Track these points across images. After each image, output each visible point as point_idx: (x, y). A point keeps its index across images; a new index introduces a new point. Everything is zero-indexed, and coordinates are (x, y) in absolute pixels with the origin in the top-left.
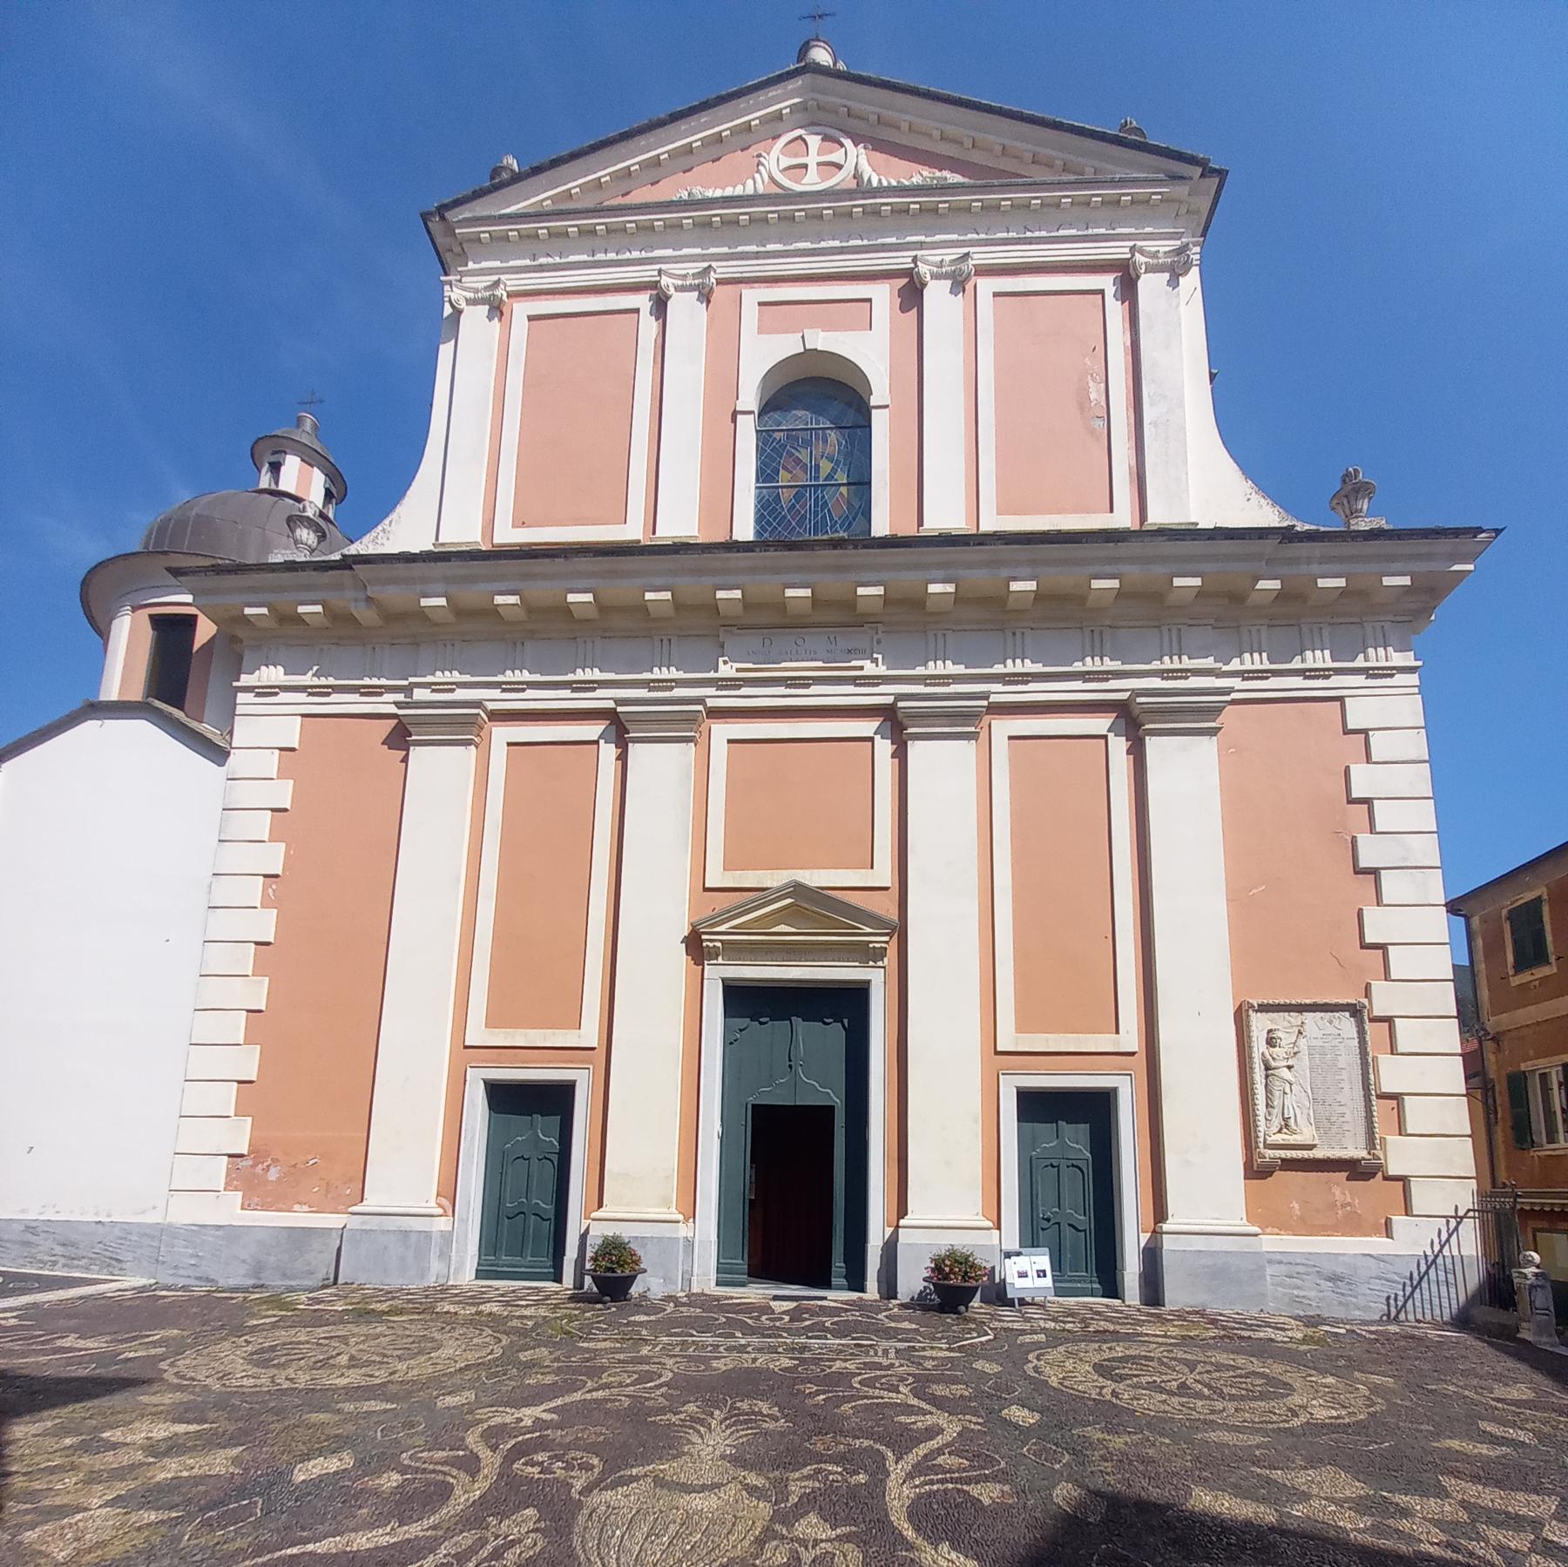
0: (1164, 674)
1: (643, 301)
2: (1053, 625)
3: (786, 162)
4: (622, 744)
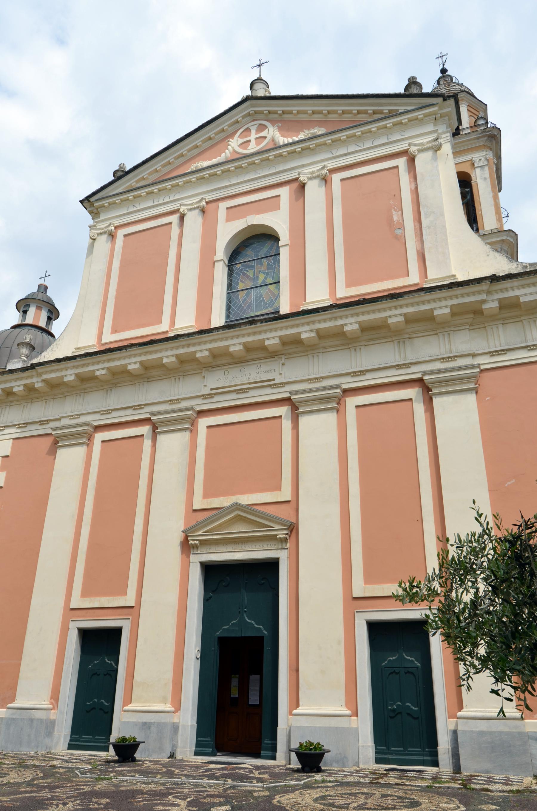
2: (376, 342)
3: (241, 141)
4: (429, 402)
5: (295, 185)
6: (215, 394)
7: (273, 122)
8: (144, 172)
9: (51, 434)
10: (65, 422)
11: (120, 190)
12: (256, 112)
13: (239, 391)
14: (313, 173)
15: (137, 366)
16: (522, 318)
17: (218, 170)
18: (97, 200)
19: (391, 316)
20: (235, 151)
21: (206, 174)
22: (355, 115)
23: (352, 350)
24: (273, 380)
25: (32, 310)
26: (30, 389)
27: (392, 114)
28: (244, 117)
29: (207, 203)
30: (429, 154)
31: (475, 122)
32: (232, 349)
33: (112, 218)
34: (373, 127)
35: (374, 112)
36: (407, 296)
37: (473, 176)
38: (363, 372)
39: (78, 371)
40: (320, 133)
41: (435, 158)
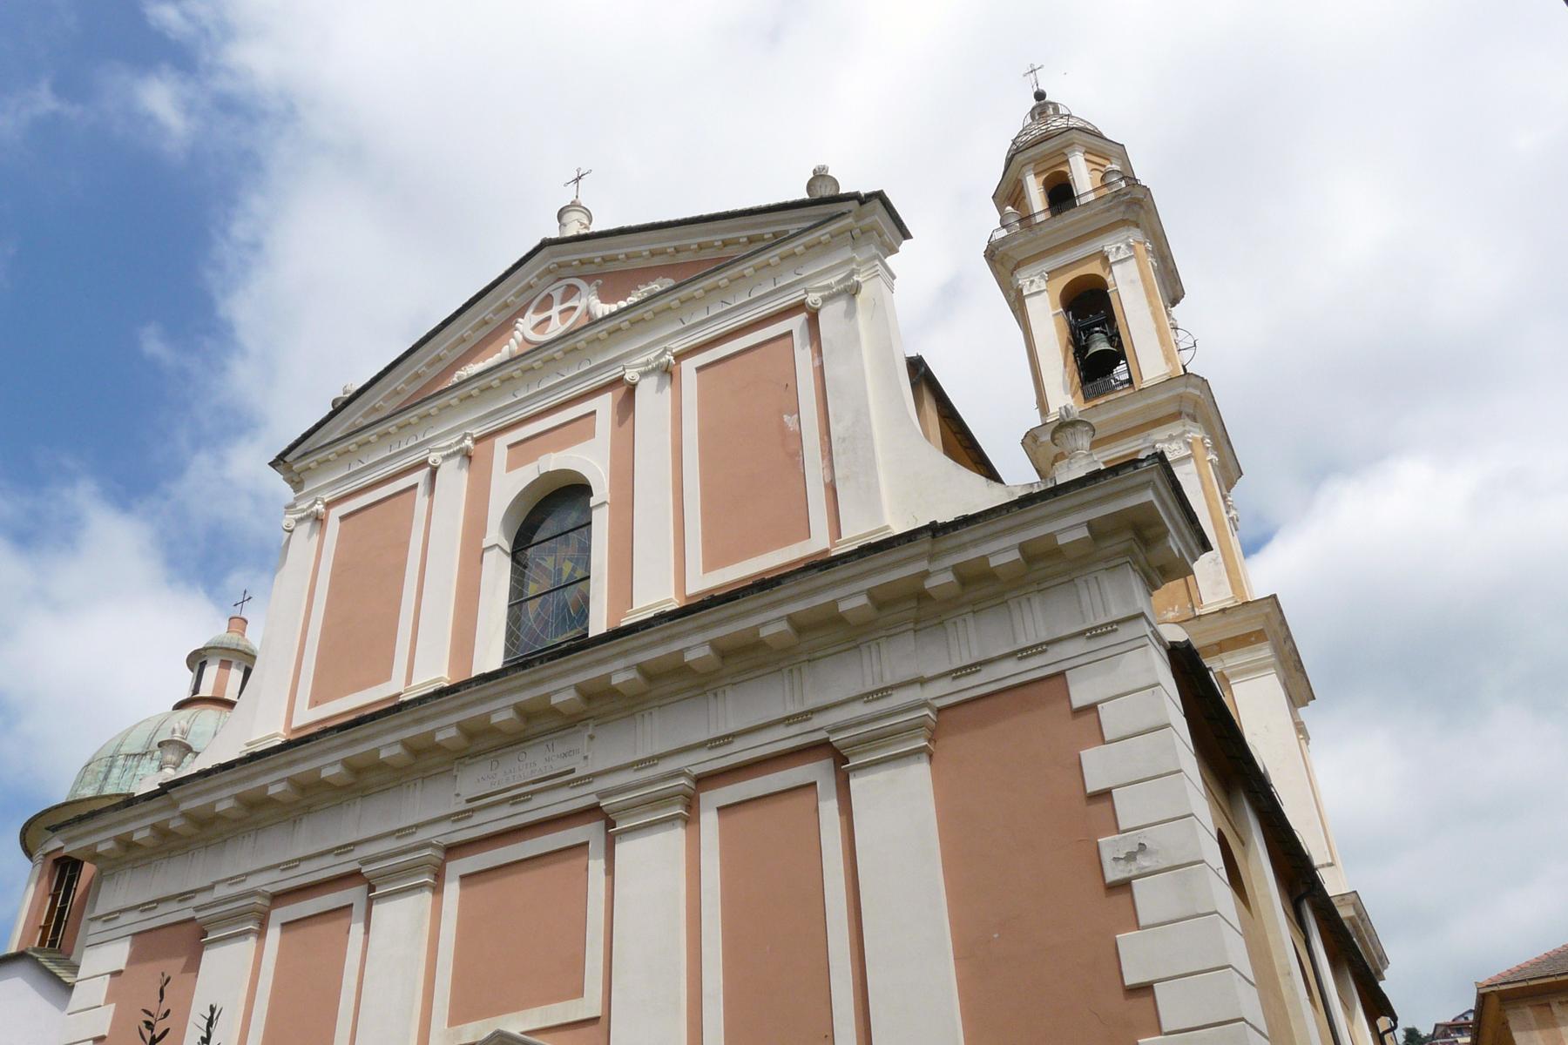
0: (232, 881)
1: (796, 323)
5: (621, 391)
6: (473, 810)
7: (589, 278)
8: (376, 398)
9: (192, 920)
10: (222, 892)
11: (337, 435)
12: (560, 266)
13: (515, 800)
14: (648, 363)
15: (453, 732)
16: (1074, 575)
17: (493, 380)
18: (305, 454)
19: (764, 624)
20: (526, 340)
21: (472, 389)
22: (695, 251)
23: (711, 697)
24: (573, 771)
25: (211, 671)
26: (162, 832)
27: (780, 239)
28: (539, 277)
29: (477, 441)
30: (840, 305)
31: (1102, 179)
32: (495, 719)
33: (323, 488)
34: (747, 268)
35: (751, 240)
36: (787, 583)
37: (1109, 280)
38: (883, 692)
39: (239, 790)
40: (659, 289)
41: (851, 313)
